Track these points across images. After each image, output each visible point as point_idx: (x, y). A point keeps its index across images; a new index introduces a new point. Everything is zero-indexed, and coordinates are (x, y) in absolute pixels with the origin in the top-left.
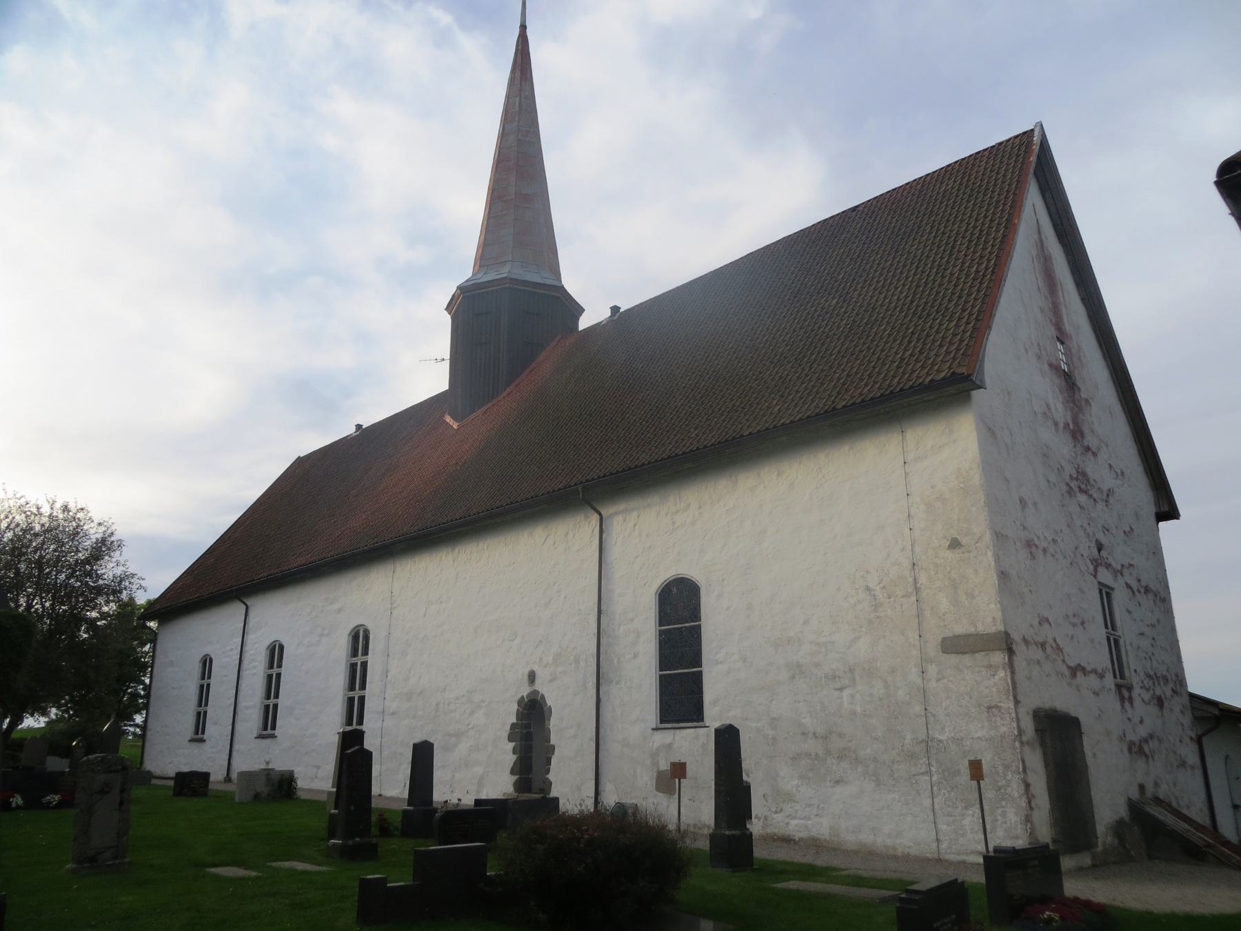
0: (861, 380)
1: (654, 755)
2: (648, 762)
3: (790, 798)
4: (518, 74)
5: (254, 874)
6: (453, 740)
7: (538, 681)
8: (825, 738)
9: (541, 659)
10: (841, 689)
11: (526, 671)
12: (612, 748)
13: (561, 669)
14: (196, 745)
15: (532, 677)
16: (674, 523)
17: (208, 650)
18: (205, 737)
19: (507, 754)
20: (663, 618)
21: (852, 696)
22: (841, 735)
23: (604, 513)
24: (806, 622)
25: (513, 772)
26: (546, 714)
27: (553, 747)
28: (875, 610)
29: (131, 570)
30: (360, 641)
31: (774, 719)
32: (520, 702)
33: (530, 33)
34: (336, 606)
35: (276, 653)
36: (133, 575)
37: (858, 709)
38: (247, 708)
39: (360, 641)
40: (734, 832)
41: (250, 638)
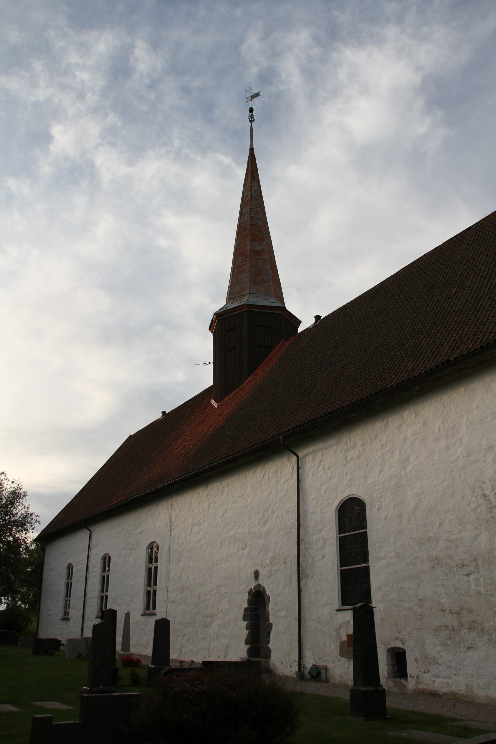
0: (468, 338)
1: (338, 630)
2: (334, 634)
3: (434, 661)
4: (249, 177)
5: (65, 707)
6: (209, 620)
7: (260, 577)
8: (458, 613)
9: (262, 561)
10: (468, 575)
11: (254, 570)
12: (309, 625)
13: (275, 568)
14: (64, 622)
15: (256, 574)
16: (346, 458)
17: (71, 561)
18: (70, 617)
19: (241, 630)
20: (341, 528)
21: (477, 580)
22: (470, 611)
23: (300, 455)
24: (441, 525)
25: (246, 643)
26: (266, 600)
27: (271, 625)
28: (491, 512)
29: (30, 511)
30: (153, 553)
31: (421, 600)
32: (250, 592)
33: (256, 152)
34: (140, 530)
35: (106, 560)
36: (32, 514)
37: (482, 590)
38: (91, 598)
39: (153, 553)
40: (368, 688)
41: (93, 552)
